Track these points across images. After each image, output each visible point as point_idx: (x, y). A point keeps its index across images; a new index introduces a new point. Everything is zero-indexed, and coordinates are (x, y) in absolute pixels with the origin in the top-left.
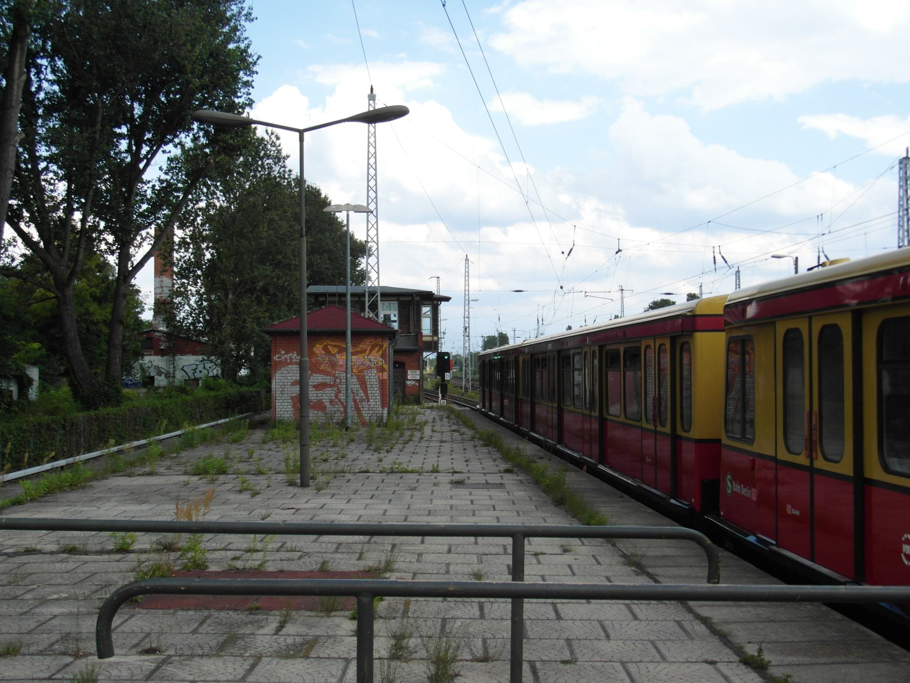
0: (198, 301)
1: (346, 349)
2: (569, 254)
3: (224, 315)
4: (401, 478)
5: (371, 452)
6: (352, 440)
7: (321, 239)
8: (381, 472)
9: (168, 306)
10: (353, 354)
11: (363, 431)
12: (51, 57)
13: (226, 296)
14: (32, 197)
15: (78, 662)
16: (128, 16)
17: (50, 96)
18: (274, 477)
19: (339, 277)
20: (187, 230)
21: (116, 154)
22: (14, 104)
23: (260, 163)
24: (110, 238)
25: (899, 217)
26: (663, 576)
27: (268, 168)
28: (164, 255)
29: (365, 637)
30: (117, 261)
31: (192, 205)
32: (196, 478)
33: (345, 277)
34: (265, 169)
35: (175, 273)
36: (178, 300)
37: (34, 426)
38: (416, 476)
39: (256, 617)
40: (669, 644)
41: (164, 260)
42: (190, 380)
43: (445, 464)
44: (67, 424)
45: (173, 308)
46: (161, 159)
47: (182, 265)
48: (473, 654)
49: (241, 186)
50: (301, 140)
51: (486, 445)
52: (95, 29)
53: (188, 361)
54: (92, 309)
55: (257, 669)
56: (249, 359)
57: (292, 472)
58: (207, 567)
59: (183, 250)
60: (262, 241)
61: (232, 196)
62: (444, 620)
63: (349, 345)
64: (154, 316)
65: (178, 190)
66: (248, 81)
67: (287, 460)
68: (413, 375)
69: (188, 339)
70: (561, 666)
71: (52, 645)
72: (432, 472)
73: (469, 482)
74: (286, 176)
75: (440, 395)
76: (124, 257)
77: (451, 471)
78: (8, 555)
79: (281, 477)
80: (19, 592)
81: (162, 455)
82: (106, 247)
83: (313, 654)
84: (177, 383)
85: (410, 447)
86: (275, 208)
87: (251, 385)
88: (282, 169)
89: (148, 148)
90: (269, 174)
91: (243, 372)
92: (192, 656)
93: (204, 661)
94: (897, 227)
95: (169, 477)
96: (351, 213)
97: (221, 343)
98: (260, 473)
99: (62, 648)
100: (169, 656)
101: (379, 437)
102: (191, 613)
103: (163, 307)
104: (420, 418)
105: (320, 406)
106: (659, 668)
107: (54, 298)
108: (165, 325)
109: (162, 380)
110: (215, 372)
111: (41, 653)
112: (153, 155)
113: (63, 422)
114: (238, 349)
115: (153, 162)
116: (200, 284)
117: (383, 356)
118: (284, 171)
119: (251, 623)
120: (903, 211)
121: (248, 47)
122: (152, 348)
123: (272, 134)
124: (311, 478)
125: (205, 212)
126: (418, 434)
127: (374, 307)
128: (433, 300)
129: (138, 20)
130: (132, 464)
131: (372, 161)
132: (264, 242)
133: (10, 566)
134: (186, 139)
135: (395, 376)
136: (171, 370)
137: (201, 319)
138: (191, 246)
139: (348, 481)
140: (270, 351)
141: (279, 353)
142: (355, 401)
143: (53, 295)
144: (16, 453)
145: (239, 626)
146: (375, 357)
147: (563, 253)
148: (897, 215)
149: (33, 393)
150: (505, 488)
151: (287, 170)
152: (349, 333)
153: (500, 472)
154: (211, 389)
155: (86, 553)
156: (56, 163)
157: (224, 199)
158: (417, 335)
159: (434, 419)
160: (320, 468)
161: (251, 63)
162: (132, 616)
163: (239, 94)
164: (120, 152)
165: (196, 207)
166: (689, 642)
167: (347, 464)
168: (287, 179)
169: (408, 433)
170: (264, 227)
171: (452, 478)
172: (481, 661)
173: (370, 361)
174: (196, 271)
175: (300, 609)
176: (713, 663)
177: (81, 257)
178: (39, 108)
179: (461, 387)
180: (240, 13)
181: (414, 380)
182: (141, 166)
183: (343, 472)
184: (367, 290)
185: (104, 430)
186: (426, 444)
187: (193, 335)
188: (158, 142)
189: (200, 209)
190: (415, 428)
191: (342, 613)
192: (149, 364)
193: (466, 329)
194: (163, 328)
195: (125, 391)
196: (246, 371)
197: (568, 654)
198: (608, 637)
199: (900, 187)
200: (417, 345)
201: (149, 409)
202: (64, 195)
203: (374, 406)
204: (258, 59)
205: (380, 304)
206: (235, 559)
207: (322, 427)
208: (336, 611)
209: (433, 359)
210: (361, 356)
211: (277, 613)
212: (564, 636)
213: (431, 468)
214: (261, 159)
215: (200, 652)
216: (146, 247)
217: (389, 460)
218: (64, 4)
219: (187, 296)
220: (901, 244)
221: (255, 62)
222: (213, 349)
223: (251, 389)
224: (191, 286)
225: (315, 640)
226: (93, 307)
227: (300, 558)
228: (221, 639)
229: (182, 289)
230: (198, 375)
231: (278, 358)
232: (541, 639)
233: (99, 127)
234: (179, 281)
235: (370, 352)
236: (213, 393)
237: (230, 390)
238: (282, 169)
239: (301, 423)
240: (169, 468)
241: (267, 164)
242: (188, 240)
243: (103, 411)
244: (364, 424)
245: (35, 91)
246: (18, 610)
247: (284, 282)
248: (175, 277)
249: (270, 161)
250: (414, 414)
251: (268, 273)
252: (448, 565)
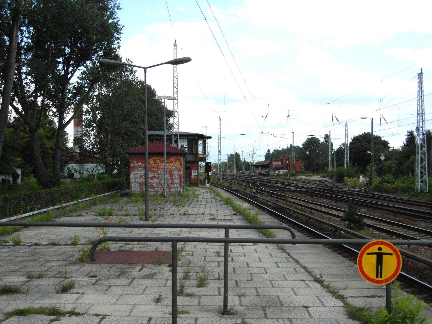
0: (95, 138)
1: (164, 161)
2: (266, 117)
3: (107, 145)
4: (188, 217)
5: (175, 207)
6: (167, 202)
7: (151, 109)
8: (179, 215)
9: (80, 141)
10: (167, 163)
11: (171, 198)
12: (28, 26)
13: (108, 136)
14: (19, 91)
15: (66, 280)
16: (64, 8)
17: (28, 45)
18: (133, 217)
19: (160, 127)
20: (89, 105)
21: (57, 71)
22: (13, 50)
23: (123, 74)
24: (55, 110)
25: (418, 100)
26: (292, 253)
27: (127, 76)
28: (78, 117)
29: (174, 272)
30: (58, 120)
31: (91, 94)
32: (99, 218)
33: (163, 127)
34: (126, 77)
35: (84, 125)
36: (85, 138)
37: (23, 196)
38: (195, 217)
39: (132, 266)
40: (289, 275)
41: (78, 119)
42: (90, 175)
43: (207, 211)
44: (37, 195)
45: (83, 141)
46: (78, 73)
47: (87, 122)
48: (214, 277)
49: (115, 85)
50: (145, 72)
51: (226, 204)
52: (49, 14)
53: (89, 166)
54: (45, 142)
55: (133, 282)
56: (118, 165)
57: (141, 215)
58: (110, 250)
59: (87, 115)
60: (124, 110)
61: (110, 89)
62: (204, 267)
63: (165, 159)
64: (74, 145)
65: (86, 87)
66: (118, 37)
67: (139, 210)
68: (194, 173)
69: (90, 156)
70: (247, 281)
71: (55, 275)
72: (202, 215)
73: (218, 219)
74: (135, 80)
75: (207, 182)
76: (61, 119)
77: (210, 214)
78: (28, 246)
79: (136, 217)
80: (37, 258)
81: (83, 208)
82: (52, 114)
83: (154, 278)
84: (84, 176)
85: (192, 205)
86: (130, 95)
87: (119, 178)
88: (133, 77)
89: (72, 68)
90: (127, 79)
91: (115, 171)
92: (109, 278)
93: (114, 280)
94: (417, 105)
95: (88, 217)
96: (166, 100)
97: (105, 158)
98: (127, 215)
99: (60, 276)
100: (100, 278)
101: (178, 201)
102: (106, 265)
103: (78, 141)
104: (197, 193)
105: (152, 187)
106: (283, 282)
107: (29, 137)
108: (79, 149)
109: (77, 175)
110: (102, 171)
111: (52, 277)
112: (75, 72)
113: (35, 194)
114: (113, 160)
115: (74, 75)
116: (95, 130)
117: (180, 164)
118: (134, 78)
119: (130, 268)
120: (420, 97)
121: (118, 21)
122: (72, 160)
123: (129, 60)
124: (150, 217)
125: (98, 97)
126: (196, 199)
127: (176, 142)
128: (204, 138)
129: (68, 10)
130: (71, 212)
131: (175, 85)
132: (125, 111)
133: (31, 250)
134: (89, 64)
135: (186, 173)
136: (82, 170)
137: (96, 147)
138: (91, 113)
139: (166, 218)
140: (129, 162)
141: (134, 163)
142: (168, 184)
143: (29, 136)
144: (15, 208)
145: (125, 269)
146: (177, 165)
147: (263, 117)
148: (417, 99)
149: (19, 181)
150: (233, 221)
151: (136, 77)
152: (165, 154)
153: (231, 215)
154: (101, 179)
155: (60, 245)
156: (31, 75)
157: (106, 91)
158: (196, 154)
159: (204, 193)
160: (153, 213)
161: (120, 29)
162: (83, 266)
163: (114, 43)
164: (59, 70)
165: (93, 94)
166: (297, 275)
167: (165, 211)
168: (136, 81)
169: (192, 199)
170: (125, 104)
171: (210, 217)
172: (217, 280)
173: (175, 167)
174: (93, 124)
175: (149, 264)
176: (304, 281)
177: (42, 118)
178: (22, 50)
179: (217, 179)
180: (114, 6)
181: (195, 175)
182: (69, 76)
183: (163, 215)
184: (173, 134)
185: (53, 198)
186: (200, 203)
187: (92, 154)
188: (77, 66)
189: (95, 96)
190: (195, 197)
191: (165, 265)
192: (71, 168)
193: (219, 151)
194: (78, 151)
195: (61, 180)
196: (117, 171)
197: (250, 278)
198: (266, 273)
199: (418, 86)
200: (196, 159)
201: (73, 188)
202: (34, 90)
203: (176, 187)
204: (123, 27)
205: (179, 140)
206: (121, 247)
207: (153, 196)
208: (162, 264)
209: (204, 165)
210: (170, 164)
211: (139, 265)
212: (250, 272)
213: (201, 213)
214: (124, 72)
215: (112, 277)
216: (71, 114)
217: (183, 210)
218: (34, 1)
219: (89, 136)
220: (418, 113)
221: (122, 29)
222: (102, 161)
223: (119, 179)
224: (91, 131)
225: (155, 274)
226: (46, 141)
227: (147, 246)
228: (119, 273)
229: (87, 133)
230: (94, 173)
231: (133, 165)
232: (240, 273)
233: (50, 59)
234: (85, 129)
235: (175, 162)
236: (102, 181)
237: (109, 180)
238: (133, 77)
239: (144, 195)
240: (87, 213)
241: (127, 74)
242: (90, 110)
243: (53, 189)
244: (172, 195)
245: (20, 42)
246: (39, 264)
247: (135, 130)
248: (83, 127)
249: (128, 73)
250: (195, 191)
251: (127, 125)
252: (207, 249)
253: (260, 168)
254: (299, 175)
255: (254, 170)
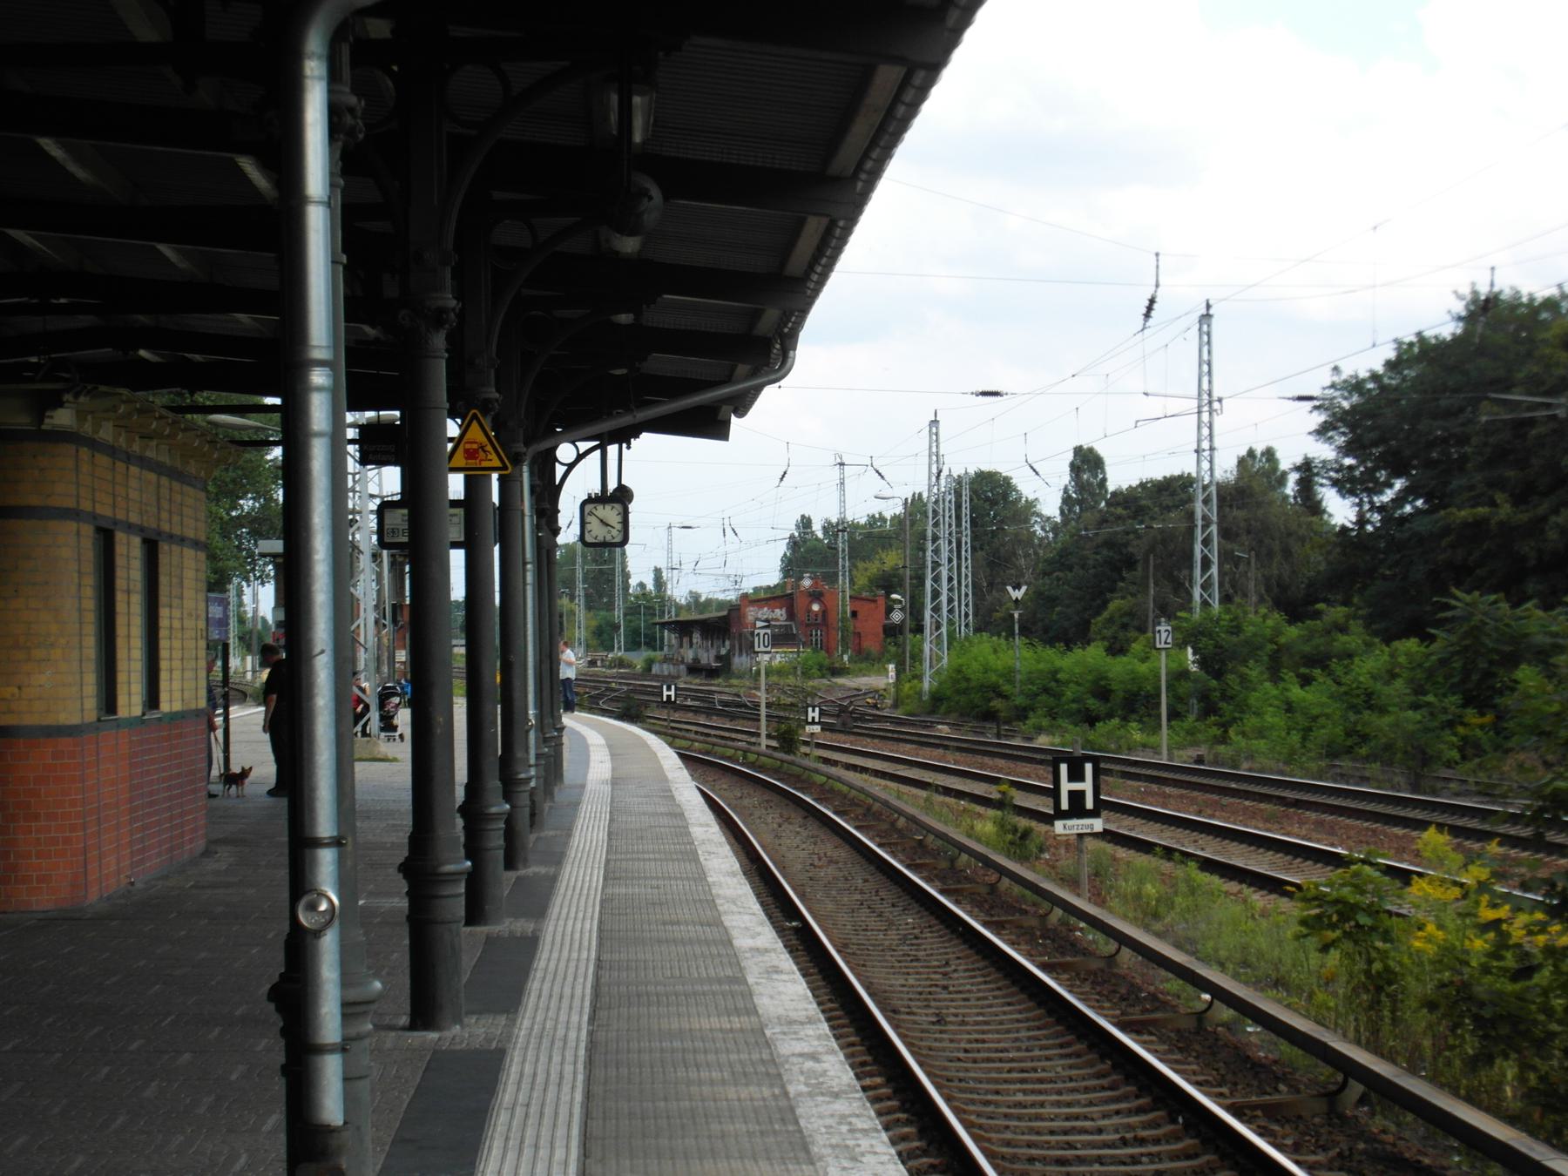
253: (697, 637)
254: (861, 673)
255: (670, 646)
